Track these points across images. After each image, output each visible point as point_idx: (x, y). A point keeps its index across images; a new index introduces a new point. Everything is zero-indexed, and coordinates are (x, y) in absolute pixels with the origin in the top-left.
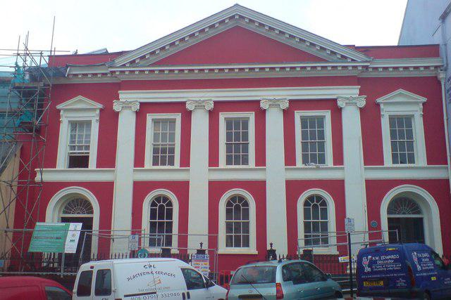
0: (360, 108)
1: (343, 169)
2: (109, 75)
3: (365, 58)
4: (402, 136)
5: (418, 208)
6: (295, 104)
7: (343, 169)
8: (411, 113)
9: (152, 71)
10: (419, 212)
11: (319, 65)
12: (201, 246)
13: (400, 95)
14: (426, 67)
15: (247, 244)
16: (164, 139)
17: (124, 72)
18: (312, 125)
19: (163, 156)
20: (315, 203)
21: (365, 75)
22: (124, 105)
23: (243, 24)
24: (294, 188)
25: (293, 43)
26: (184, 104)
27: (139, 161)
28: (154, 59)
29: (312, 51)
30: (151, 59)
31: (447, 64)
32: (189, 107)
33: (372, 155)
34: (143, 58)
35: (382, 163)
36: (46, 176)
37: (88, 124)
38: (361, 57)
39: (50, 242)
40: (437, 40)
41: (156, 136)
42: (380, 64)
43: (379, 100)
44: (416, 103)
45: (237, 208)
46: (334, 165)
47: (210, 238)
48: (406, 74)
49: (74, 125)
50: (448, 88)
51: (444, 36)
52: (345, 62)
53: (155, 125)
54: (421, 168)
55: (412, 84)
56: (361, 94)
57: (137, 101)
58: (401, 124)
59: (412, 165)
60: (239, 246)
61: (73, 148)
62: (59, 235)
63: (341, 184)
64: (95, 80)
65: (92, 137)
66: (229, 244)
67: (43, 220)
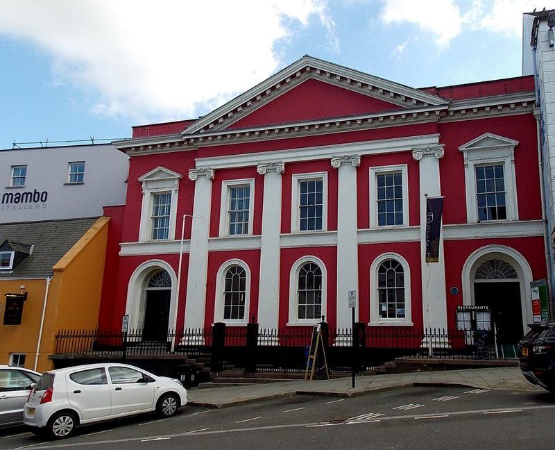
4: (390, 195)
10: (515, 276)
14: (517, 104)
17: (198, 139)
21: (446, 120)
25: (366, 92)
28: (229, 122)
32: (334, 164)
34: (216, 122)
36: (126, 250)
37: (168, 195)
38: (436, 100)
42: (462, 106)
48: (494, 114)
49: (156, 196)
52: (421, 108)
55: (501, 126)
56: (440, 142)
58: (490, 174)
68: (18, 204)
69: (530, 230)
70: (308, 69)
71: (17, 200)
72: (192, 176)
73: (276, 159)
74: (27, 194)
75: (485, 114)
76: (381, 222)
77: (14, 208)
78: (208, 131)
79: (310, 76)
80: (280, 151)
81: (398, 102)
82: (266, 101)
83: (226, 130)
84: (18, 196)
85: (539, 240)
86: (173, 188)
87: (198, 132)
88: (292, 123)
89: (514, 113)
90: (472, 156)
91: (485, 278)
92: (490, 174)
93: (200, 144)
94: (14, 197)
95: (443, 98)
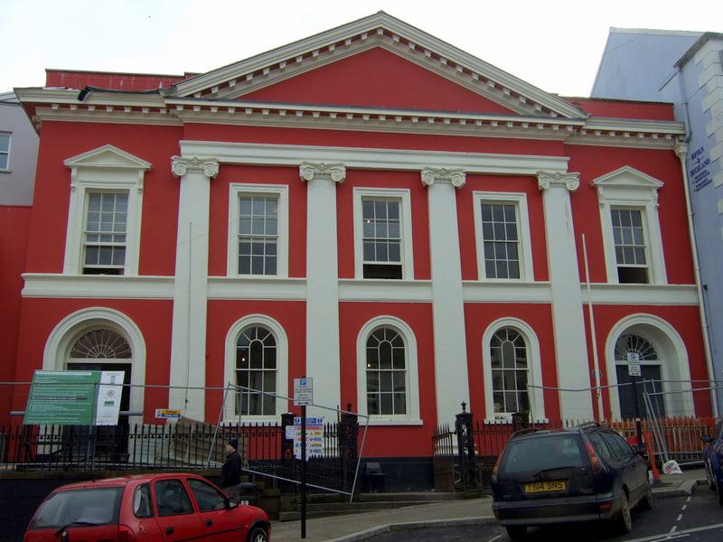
0: (337, 183)
1: (430, 284)
2: (163, 112)
3: (577, 113)
5: (652, 350)
6: (357, 175)
7: (305, 282)
9: (242, 110)
11: (495, 119)
12: (464, 409)
13: (626, 174)
14: (661, 135)
15: (401, 409)
16: (258, 228)
17: (190, 107)
18: (500, 217)
19: (257, 259)
20: (261, 342)
21: (576, 141)
22: (190, 166)
23: (389, 45)
24: (476, 316)
25: (467, 83)
26: (296, 169)
27: (217, 265)
28: (242, 89)
29: (498, 97)
30: (237, 89)
31: (691, 133)
32: (304, 174)
33: (592, 268)
34: (224, 86)
35: (605, 280)
39: (64, 406)
40: (665, 97)
41: (243, 221)
44: (649, 189)
45: (385, 347)
46: (140, 274)
47: (209, 395)
49: (93, 195)
50: (692, 167)
51: (683, 91)
53: (90, 200)
54: (659, 290)
57: (461, 170)
61: (90, 237)
62: (82, 394)
63: (166, 307)
64: (138, 119)
65: (128, 219)
66: (242, 410)
67: (40, 367)
69: (681, 297)
70: (380, 32)
72: (177, 168)
73: (332, 160)
75: (262, 120)
76: (243, 269)
78: (208, 96)
79: (378, 42)
80: (462, 153)
81: (513, 104)
82: (308, 66)
85: (694, 310)
86: (134, 186)
87: (191, 97)
88: (489, 115)
92: (627, 218)
93: (189, 118)
95: (581, 110)
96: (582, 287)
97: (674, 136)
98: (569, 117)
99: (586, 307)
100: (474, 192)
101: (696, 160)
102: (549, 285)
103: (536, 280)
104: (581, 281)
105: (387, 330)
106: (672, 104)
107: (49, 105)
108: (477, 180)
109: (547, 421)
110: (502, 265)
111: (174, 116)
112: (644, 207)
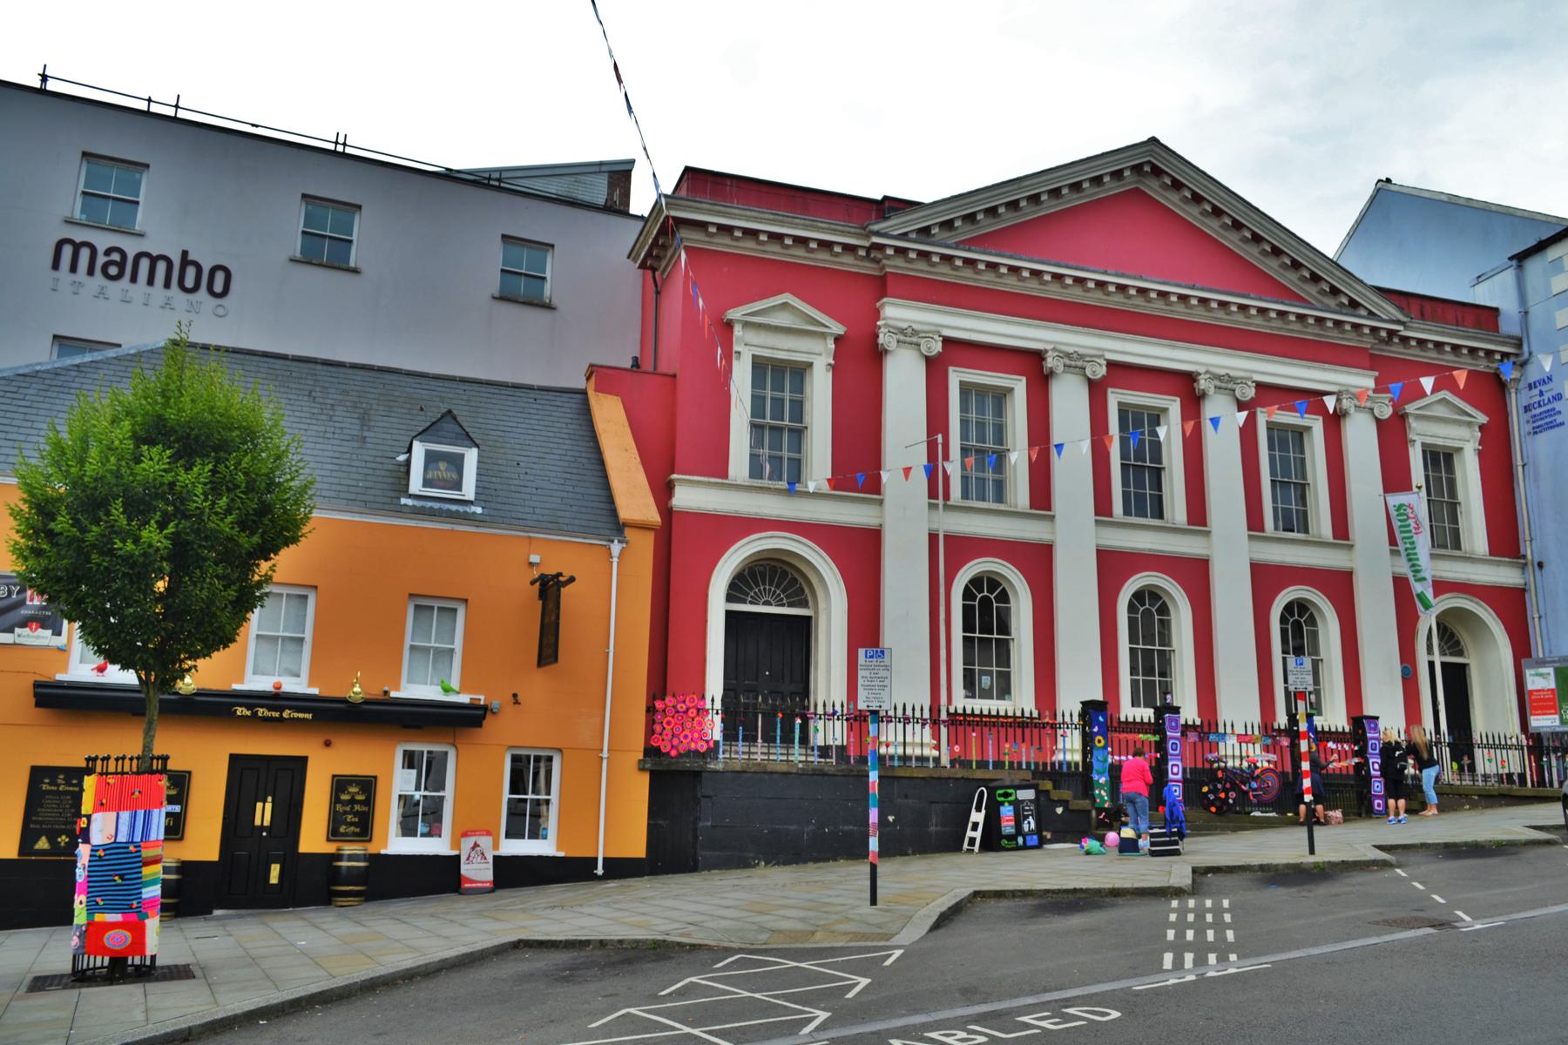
5: (1458, 643)
8: (1457, 444)
34: (948, 225)
43: (734, 314)
45: (986, 602)
59: (1002, 507)
60: (1139, 706)
68: (193, 297)
71: (113, 271)
74: (154, 260)
77: (101, 294)
83: (957, 246)
84: (116, 257)
87: (904, 236)
89: (833, 262)
90: (753, 337)
91: (744, 601)
94: (101, 260)
95: (1401, 309)
96: (932, 507)
97: (1505, 355)
98: (1384, 317)
99: (933, 538)
100: (951, 369)
101: (1536, 392)
102: (1352, 546)
103: (1335, 538)
104: (929, 498)
105: (989, 579)
106: (1496, 310)
107: (703, 225)
108: (1121, 372)
109: (1198, 722)
110: (1140, 499)
111: (877, 261)
112: (811, 365)
